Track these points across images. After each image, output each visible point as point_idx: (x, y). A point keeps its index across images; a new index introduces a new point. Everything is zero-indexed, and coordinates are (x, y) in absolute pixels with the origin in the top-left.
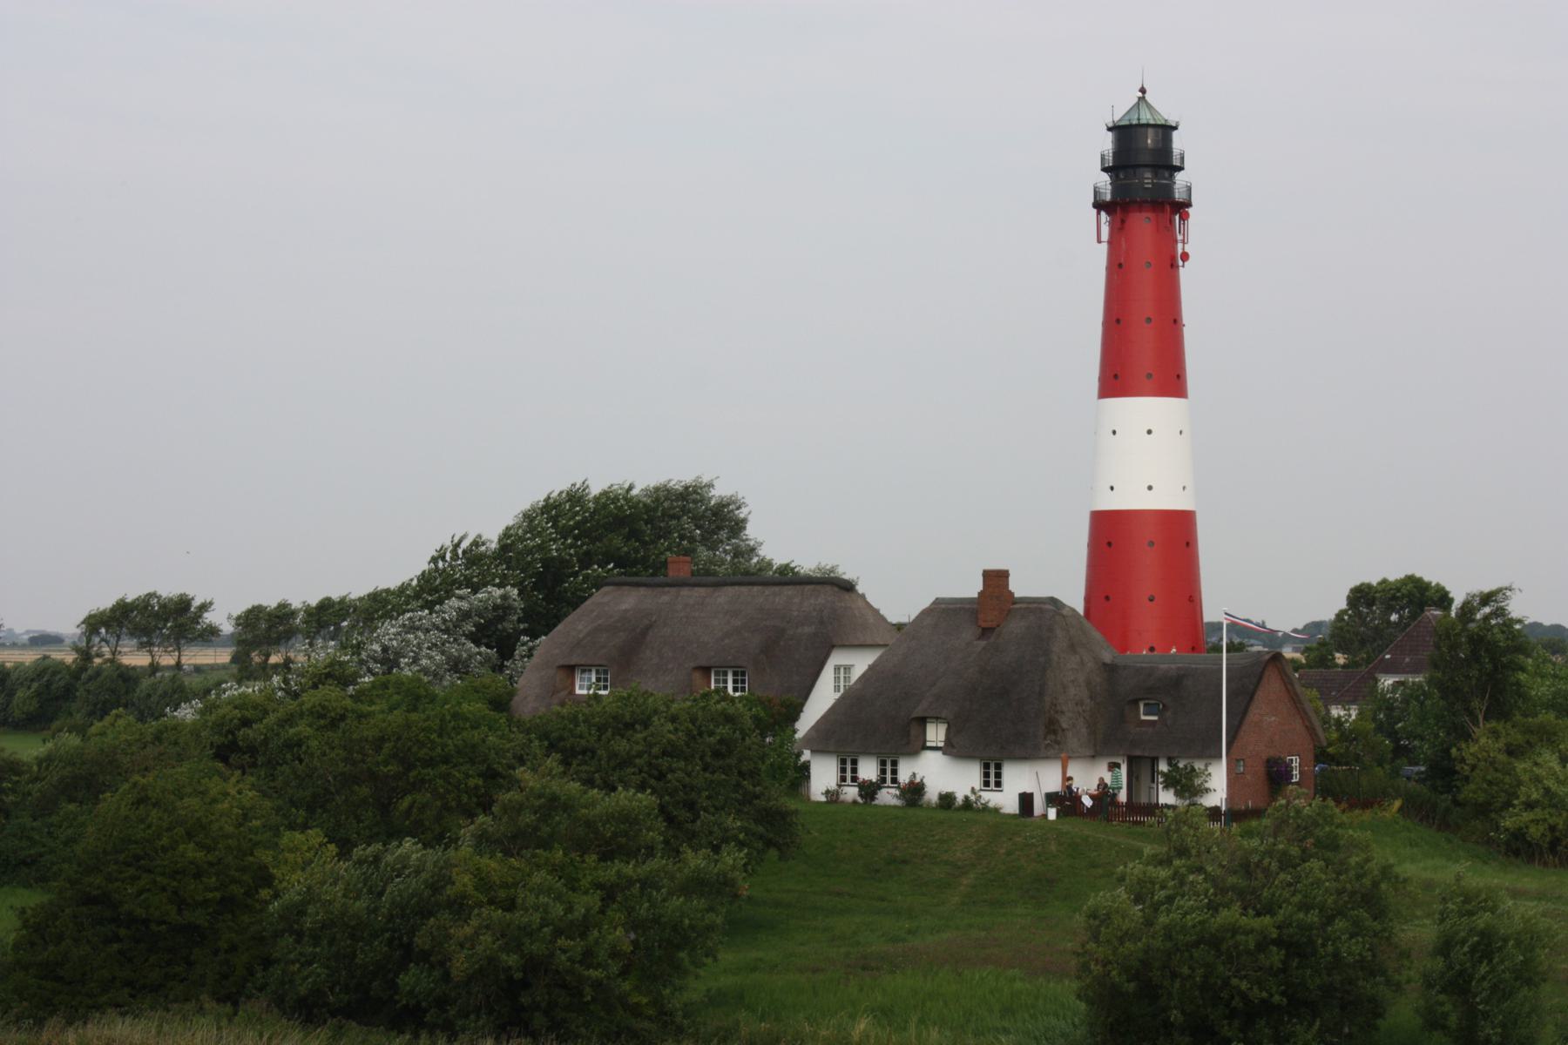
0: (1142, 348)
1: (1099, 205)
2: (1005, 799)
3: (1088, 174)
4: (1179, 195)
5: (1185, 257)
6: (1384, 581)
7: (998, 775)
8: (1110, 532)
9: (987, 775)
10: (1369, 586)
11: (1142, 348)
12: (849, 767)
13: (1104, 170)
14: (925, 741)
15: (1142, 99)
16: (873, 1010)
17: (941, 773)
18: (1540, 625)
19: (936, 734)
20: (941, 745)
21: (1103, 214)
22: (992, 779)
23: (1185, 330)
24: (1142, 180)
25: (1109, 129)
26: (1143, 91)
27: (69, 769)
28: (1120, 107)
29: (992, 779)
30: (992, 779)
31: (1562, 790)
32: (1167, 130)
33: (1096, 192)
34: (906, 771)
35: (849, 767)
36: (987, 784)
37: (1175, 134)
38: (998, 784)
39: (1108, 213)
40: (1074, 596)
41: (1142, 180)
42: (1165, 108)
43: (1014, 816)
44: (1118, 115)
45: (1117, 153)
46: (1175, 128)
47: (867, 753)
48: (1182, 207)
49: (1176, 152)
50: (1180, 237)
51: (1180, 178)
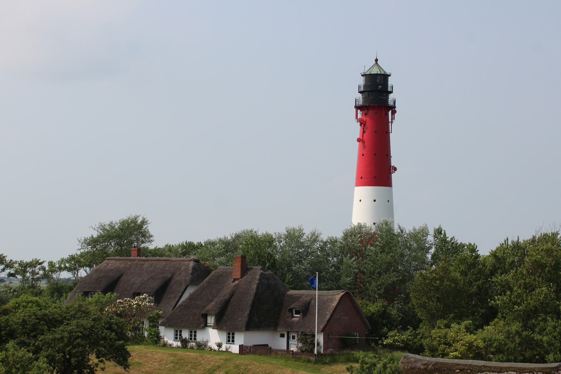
0: (377, 168)
1: (357, 108)
3: (352, 92)
4: (391, 103)
6: (293, 237)
7: (233, 338)
10: (269, 241)
11: (377, 168)
13: (360, 92)
15: (377, 63)
16: (516, 319)
19: (211, 320)
20: (212, 325)
21: (359, 111)
22: (231, 339)
24: (376, 99)
25: (362, 76)
26: (376, 60)
28: (368, 66)
29: (231, 339)
30: (231, 340)
31: (375, 373)
32: (385, 77)
34: (200, 336)
35: (193, 334)
36: (229, 341)
37: (389, 78)
38: (233, 341)
39: (361, 111)
41: (376, 99)
44: (366, 70)
46: (390, 76)
47: (185, 327)
49: (389, 85)
50: (390, 120)
51: (391, 96)
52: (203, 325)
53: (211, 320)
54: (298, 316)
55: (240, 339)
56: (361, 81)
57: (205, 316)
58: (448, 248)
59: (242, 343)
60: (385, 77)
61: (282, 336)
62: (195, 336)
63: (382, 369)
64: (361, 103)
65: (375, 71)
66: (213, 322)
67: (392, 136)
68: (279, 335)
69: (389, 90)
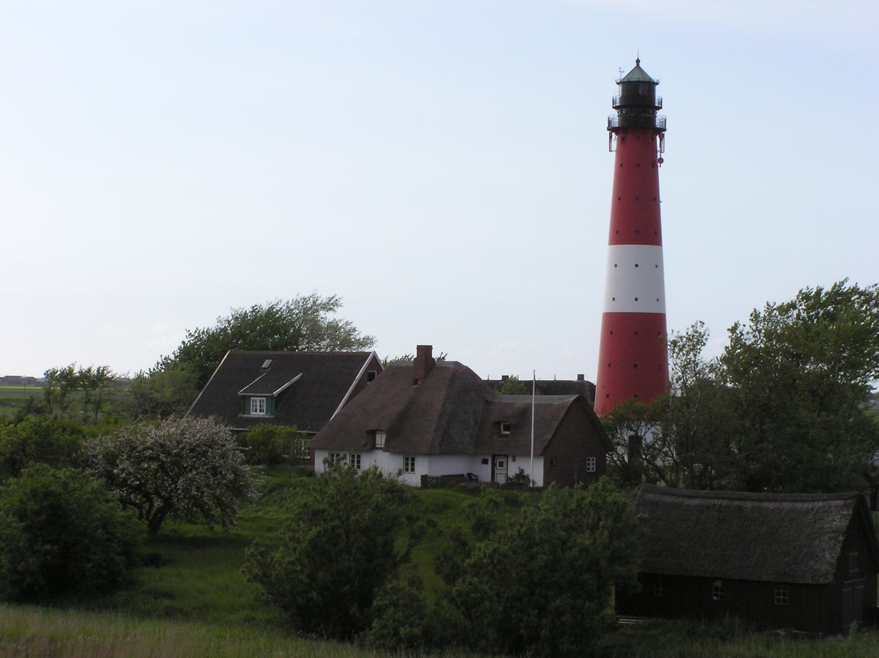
1: (611, 129)
2: (413, 479)
3: (603, 106)
4: (658, 124)
5: (661, 161)
7: (413, 465)
8: (420, 348)
9: (407, 464)
12: (356, 459)
14: (375, 444)
17: (384, 463)
18: (93, 384)
19: (381, 440)
21: (613, 134)
23: (661, 204)
24: (638, 114)
25: (618, 84)
26: (638, 61)
27: (33, 418)
30: (409, 466)
33: (610, 122)
35: (356, 459)
37: (657, 87)
38: (413, 470)
39: (616, 134)
40: (592, 377)
41: (638, 114)
42: (652, 71)
43: (416, 488)
45: (624, 98)
48: (661, 131)
50: (658, 149)
51: (659, 114)
52: (368, 447)
53: (381, 440)
54: (508, 433)
55: (423, 467)
56: (617, 92)
57: (373, 433)
58: (167, 364)
59: (425, 472)
60: (651, 85)
61: (485, 462)
62: (359, 462)
63: (454, 643)
64: (616, 124)
65: (635, 78)
66: (383, 442)
67: (663, 171)
68: (480, 461)
69: (657, 105)
